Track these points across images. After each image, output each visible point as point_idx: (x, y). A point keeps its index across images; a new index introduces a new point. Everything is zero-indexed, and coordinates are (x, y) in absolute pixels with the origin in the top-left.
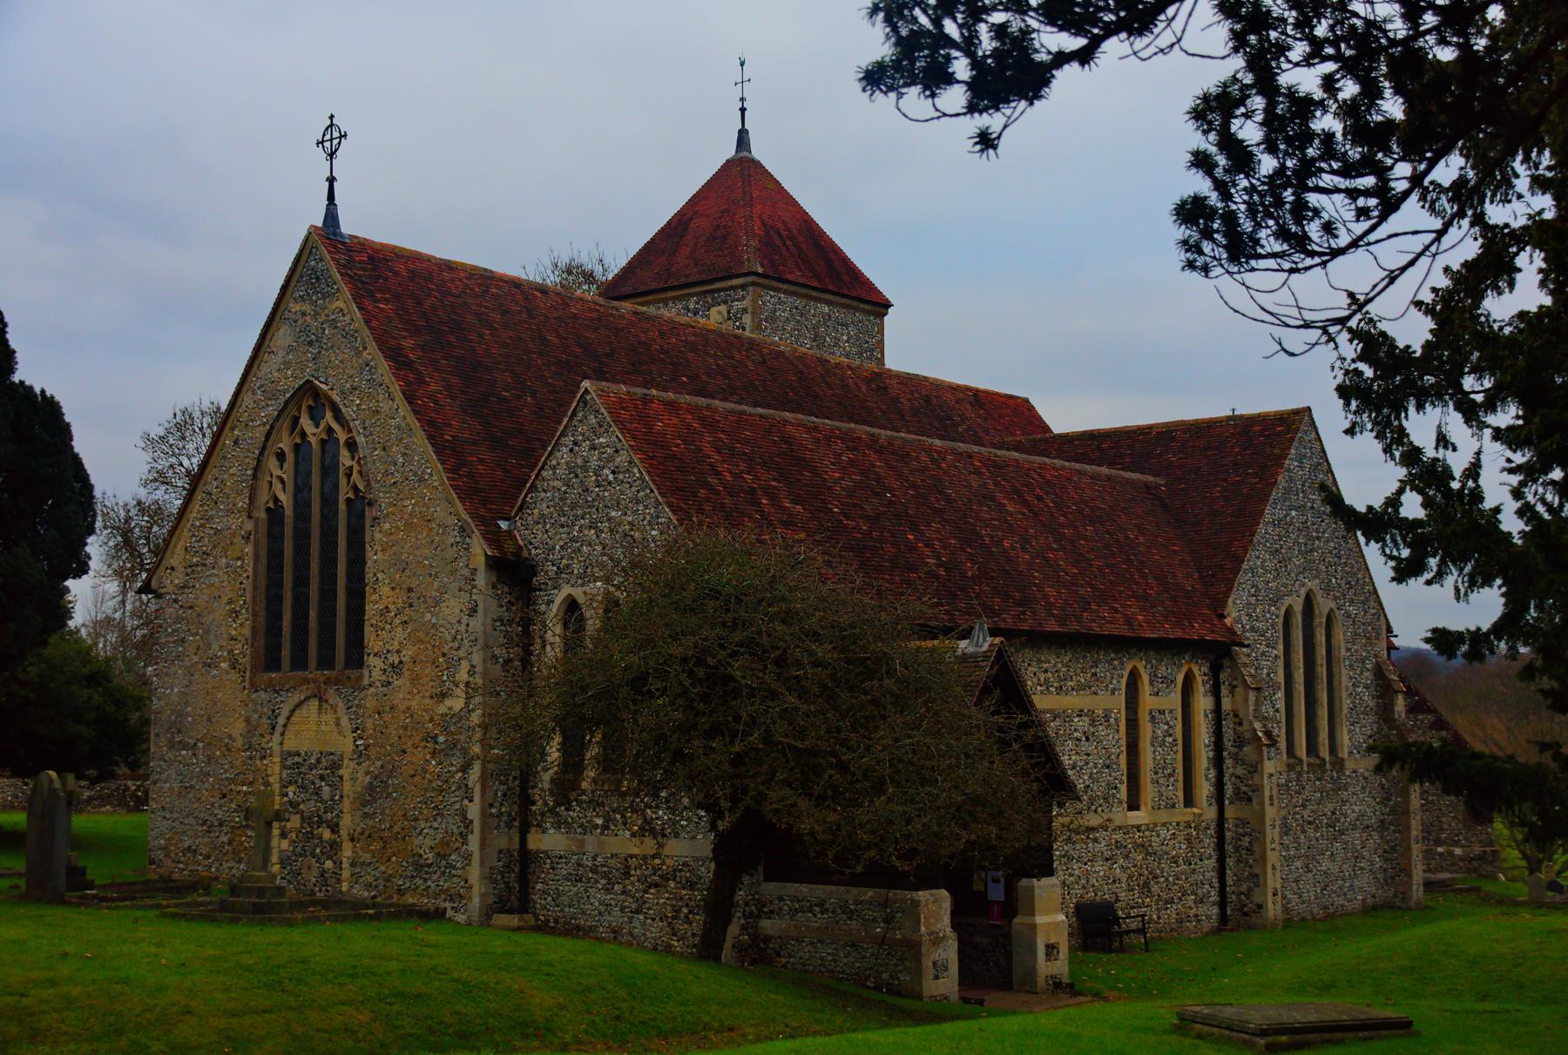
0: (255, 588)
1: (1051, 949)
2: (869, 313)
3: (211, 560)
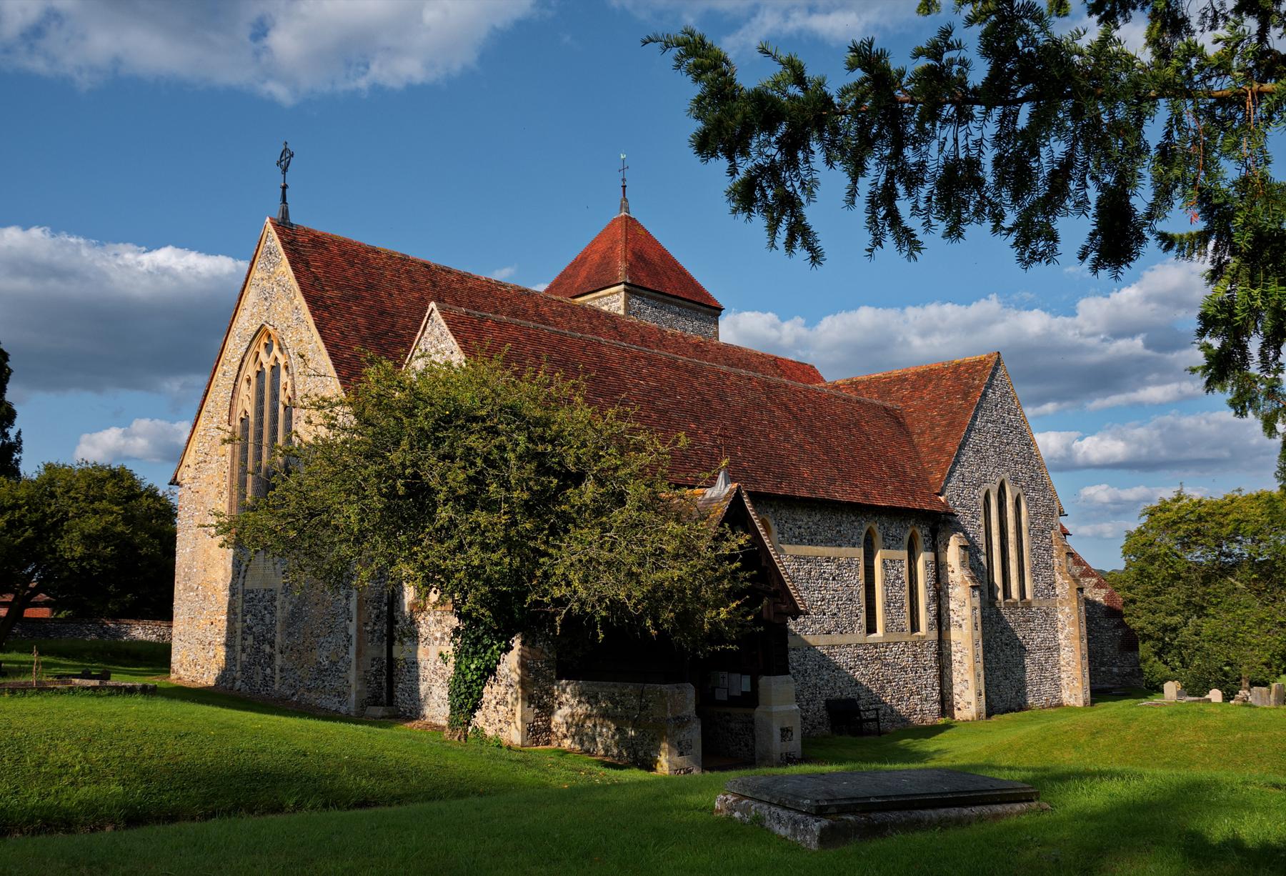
0: (232, 475)
1: (786, 732)
2: (708, 313)
3: (208, 458)
